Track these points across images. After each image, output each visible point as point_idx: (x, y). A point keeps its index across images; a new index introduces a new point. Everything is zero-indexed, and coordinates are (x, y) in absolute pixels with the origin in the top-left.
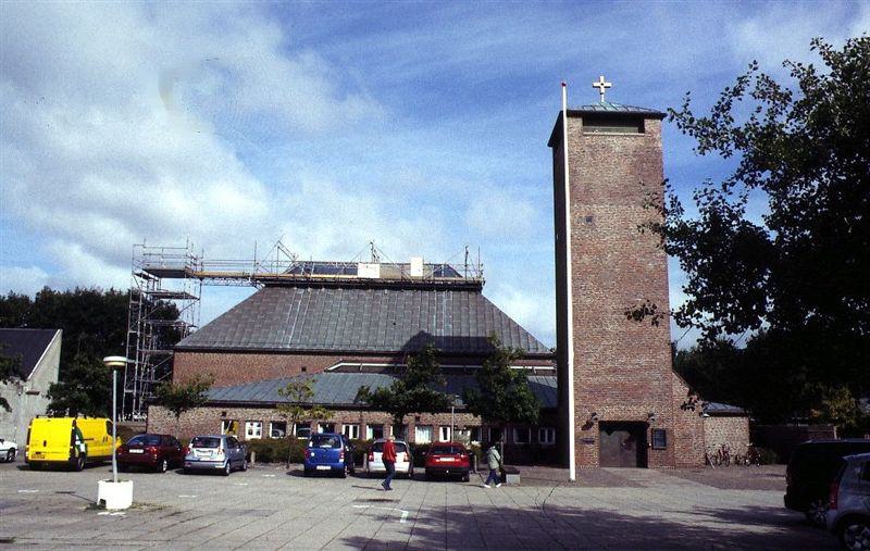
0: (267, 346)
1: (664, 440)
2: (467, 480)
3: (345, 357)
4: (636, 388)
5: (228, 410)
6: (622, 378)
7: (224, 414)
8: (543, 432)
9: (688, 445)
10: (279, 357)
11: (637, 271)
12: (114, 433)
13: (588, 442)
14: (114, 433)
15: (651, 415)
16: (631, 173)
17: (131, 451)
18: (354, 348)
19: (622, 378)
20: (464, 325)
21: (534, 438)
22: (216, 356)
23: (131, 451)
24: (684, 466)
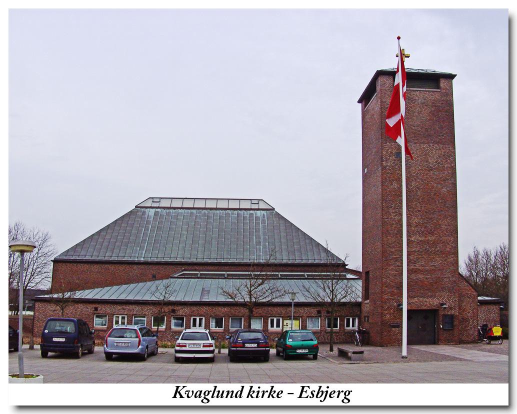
0: (126, 259)
1: (452, 323)
2: (91, 352)
3: (186, 267)
4: (431, 284)
5: (100, 307)
6: (421, 277)
7: (96, 309)
8: (348, 321)
9: (466, 326)
10: (135, 267)
11: (435, 194)
12: (21, 293)
13: (394, 327)
14: (21, 293)
15: (442, 304)
16: (430, 120)
17: (55, 339)
18: (194, 260)
19: (421, 277)
20: (277, 244)
21: (342, 325)
22: (86, 266)
23: (55, 339)
24: (337, 343)
